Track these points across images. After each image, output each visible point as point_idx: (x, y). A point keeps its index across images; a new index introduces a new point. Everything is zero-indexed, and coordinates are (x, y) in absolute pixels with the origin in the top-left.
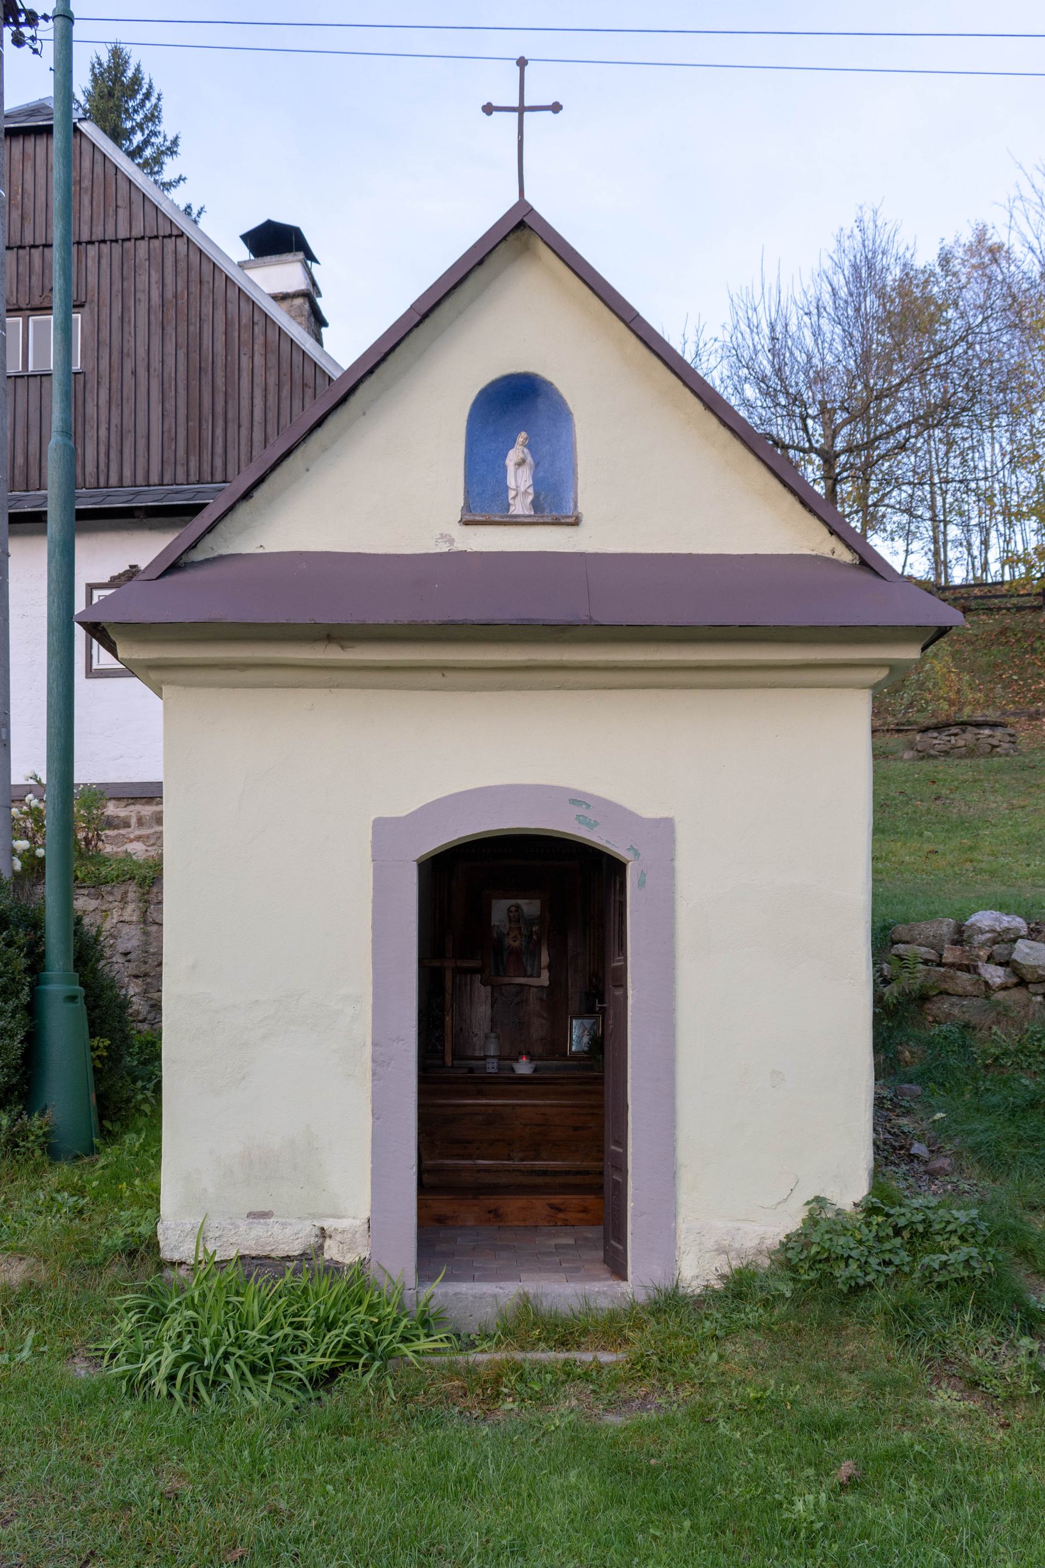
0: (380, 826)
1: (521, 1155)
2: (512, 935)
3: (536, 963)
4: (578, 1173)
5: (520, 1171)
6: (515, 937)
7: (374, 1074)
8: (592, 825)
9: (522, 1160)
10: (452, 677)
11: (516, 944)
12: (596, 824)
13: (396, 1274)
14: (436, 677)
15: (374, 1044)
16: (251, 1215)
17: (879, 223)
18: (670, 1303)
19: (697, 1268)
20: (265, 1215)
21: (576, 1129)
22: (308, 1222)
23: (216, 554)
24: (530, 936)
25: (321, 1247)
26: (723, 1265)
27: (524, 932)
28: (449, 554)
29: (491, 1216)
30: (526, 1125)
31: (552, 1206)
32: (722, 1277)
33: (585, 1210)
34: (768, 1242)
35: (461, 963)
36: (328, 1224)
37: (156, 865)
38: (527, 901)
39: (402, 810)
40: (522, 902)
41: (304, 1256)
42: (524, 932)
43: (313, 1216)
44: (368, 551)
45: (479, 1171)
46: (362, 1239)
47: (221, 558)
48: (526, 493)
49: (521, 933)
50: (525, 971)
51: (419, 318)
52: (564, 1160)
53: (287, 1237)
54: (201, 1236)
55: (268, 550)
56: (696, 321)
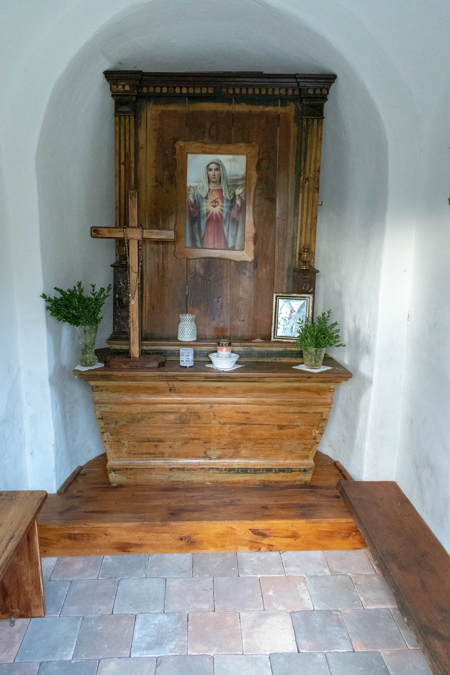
1: (219, 453)
2: (212, 198)
3: (239, 233)
4: (282, 470)
5: (217, 469)
6: (215, 201)
9: (220, 458)
11: (217, 210)
21: (281, 427)
24: (233, 201)
27: (226, 195)
29: (183, 543)
30: (225, 424)
31: (256, 532)
33: (294, 536)
35: (147, 234)
37: (315, 98)
38: (230, 157)
40: (224, 158)
42: (226, 195)
45: (171, 469)
49: (222, 197)
50: (226, 243)
51: (212, 248)
52: (266, 457)
56: (144, 236)
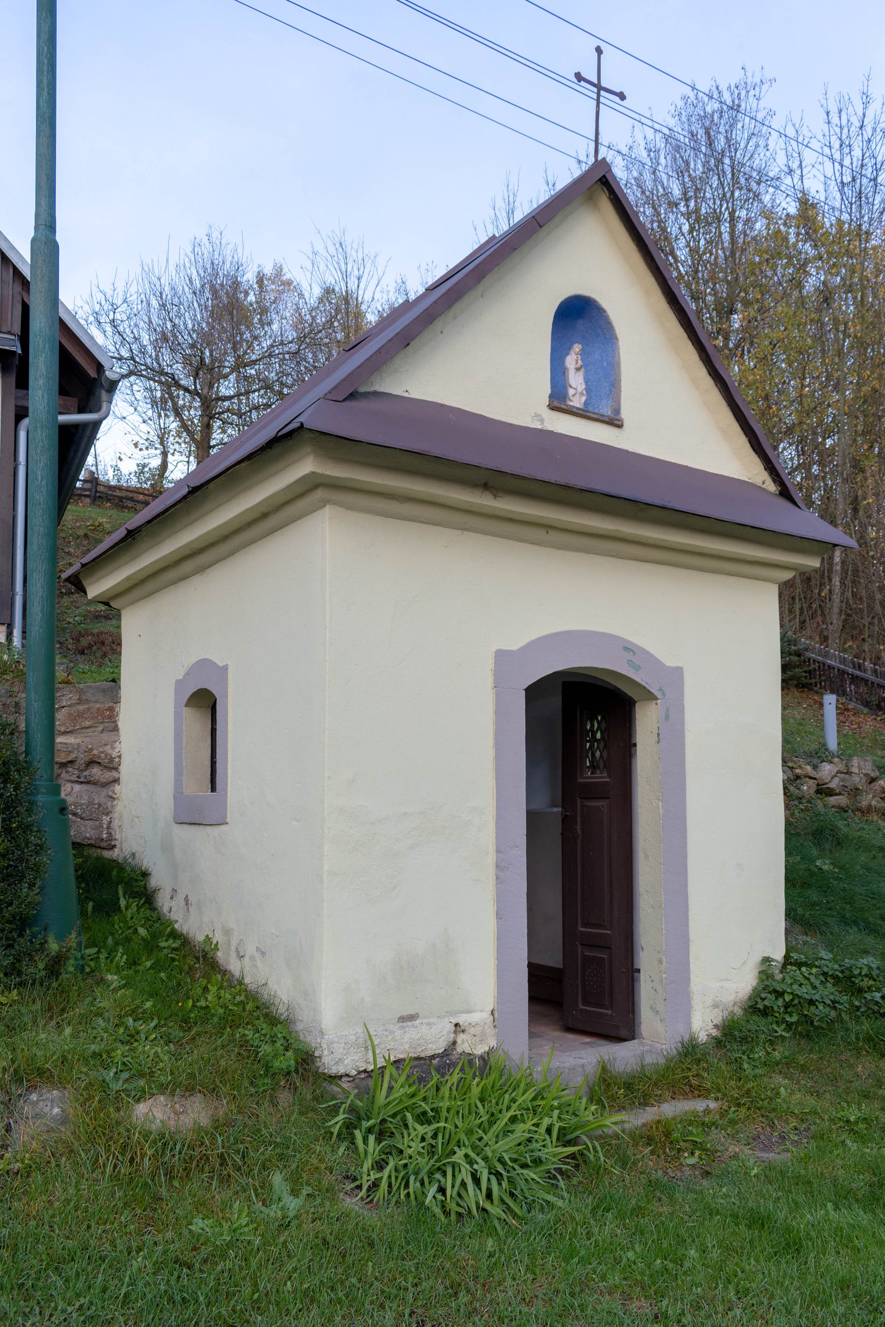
0: (500, 655)
7: (497, 878)
8: (637, 668)
10: (554, 536)
12: (640, 668)
13: (515, 1057)
14: (540, 534)
15: (498, 851)
16: (403, 1019)
17: (223, 243)
18: (690, 1051)
19: (703, 1023)
20: (412, 1018)
22: (446, 1020)
23: (372, 389)
25: (454, 1043)
26: (718, 1017)
28: (541, 430)
32: (716, 1026)
34: (740, 995)
36: (462, 1019)
39: (515, 645)
41: (446, 1053)
43: (451, 1013)
44: (488, 415)
46: (490, 1031)
47: (376, 394)
48: (582, 394)
53: (431, 1038)
54: (370, 1044)
55: (412, 396)
